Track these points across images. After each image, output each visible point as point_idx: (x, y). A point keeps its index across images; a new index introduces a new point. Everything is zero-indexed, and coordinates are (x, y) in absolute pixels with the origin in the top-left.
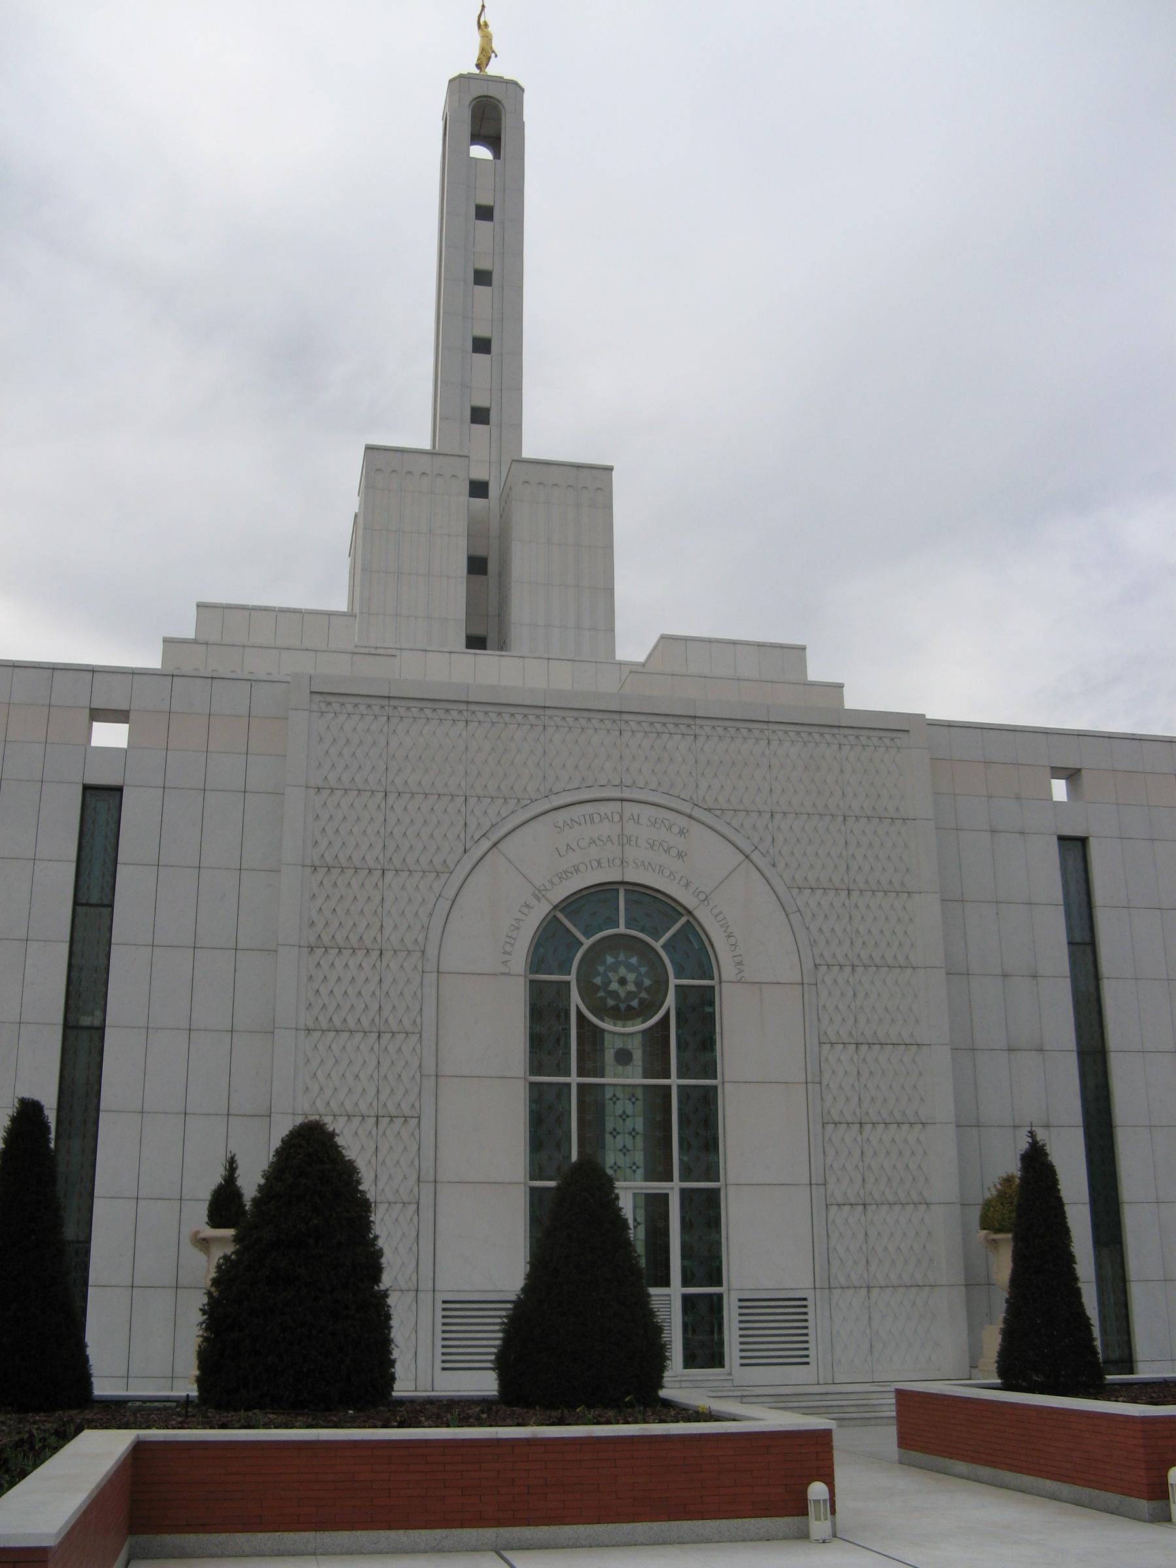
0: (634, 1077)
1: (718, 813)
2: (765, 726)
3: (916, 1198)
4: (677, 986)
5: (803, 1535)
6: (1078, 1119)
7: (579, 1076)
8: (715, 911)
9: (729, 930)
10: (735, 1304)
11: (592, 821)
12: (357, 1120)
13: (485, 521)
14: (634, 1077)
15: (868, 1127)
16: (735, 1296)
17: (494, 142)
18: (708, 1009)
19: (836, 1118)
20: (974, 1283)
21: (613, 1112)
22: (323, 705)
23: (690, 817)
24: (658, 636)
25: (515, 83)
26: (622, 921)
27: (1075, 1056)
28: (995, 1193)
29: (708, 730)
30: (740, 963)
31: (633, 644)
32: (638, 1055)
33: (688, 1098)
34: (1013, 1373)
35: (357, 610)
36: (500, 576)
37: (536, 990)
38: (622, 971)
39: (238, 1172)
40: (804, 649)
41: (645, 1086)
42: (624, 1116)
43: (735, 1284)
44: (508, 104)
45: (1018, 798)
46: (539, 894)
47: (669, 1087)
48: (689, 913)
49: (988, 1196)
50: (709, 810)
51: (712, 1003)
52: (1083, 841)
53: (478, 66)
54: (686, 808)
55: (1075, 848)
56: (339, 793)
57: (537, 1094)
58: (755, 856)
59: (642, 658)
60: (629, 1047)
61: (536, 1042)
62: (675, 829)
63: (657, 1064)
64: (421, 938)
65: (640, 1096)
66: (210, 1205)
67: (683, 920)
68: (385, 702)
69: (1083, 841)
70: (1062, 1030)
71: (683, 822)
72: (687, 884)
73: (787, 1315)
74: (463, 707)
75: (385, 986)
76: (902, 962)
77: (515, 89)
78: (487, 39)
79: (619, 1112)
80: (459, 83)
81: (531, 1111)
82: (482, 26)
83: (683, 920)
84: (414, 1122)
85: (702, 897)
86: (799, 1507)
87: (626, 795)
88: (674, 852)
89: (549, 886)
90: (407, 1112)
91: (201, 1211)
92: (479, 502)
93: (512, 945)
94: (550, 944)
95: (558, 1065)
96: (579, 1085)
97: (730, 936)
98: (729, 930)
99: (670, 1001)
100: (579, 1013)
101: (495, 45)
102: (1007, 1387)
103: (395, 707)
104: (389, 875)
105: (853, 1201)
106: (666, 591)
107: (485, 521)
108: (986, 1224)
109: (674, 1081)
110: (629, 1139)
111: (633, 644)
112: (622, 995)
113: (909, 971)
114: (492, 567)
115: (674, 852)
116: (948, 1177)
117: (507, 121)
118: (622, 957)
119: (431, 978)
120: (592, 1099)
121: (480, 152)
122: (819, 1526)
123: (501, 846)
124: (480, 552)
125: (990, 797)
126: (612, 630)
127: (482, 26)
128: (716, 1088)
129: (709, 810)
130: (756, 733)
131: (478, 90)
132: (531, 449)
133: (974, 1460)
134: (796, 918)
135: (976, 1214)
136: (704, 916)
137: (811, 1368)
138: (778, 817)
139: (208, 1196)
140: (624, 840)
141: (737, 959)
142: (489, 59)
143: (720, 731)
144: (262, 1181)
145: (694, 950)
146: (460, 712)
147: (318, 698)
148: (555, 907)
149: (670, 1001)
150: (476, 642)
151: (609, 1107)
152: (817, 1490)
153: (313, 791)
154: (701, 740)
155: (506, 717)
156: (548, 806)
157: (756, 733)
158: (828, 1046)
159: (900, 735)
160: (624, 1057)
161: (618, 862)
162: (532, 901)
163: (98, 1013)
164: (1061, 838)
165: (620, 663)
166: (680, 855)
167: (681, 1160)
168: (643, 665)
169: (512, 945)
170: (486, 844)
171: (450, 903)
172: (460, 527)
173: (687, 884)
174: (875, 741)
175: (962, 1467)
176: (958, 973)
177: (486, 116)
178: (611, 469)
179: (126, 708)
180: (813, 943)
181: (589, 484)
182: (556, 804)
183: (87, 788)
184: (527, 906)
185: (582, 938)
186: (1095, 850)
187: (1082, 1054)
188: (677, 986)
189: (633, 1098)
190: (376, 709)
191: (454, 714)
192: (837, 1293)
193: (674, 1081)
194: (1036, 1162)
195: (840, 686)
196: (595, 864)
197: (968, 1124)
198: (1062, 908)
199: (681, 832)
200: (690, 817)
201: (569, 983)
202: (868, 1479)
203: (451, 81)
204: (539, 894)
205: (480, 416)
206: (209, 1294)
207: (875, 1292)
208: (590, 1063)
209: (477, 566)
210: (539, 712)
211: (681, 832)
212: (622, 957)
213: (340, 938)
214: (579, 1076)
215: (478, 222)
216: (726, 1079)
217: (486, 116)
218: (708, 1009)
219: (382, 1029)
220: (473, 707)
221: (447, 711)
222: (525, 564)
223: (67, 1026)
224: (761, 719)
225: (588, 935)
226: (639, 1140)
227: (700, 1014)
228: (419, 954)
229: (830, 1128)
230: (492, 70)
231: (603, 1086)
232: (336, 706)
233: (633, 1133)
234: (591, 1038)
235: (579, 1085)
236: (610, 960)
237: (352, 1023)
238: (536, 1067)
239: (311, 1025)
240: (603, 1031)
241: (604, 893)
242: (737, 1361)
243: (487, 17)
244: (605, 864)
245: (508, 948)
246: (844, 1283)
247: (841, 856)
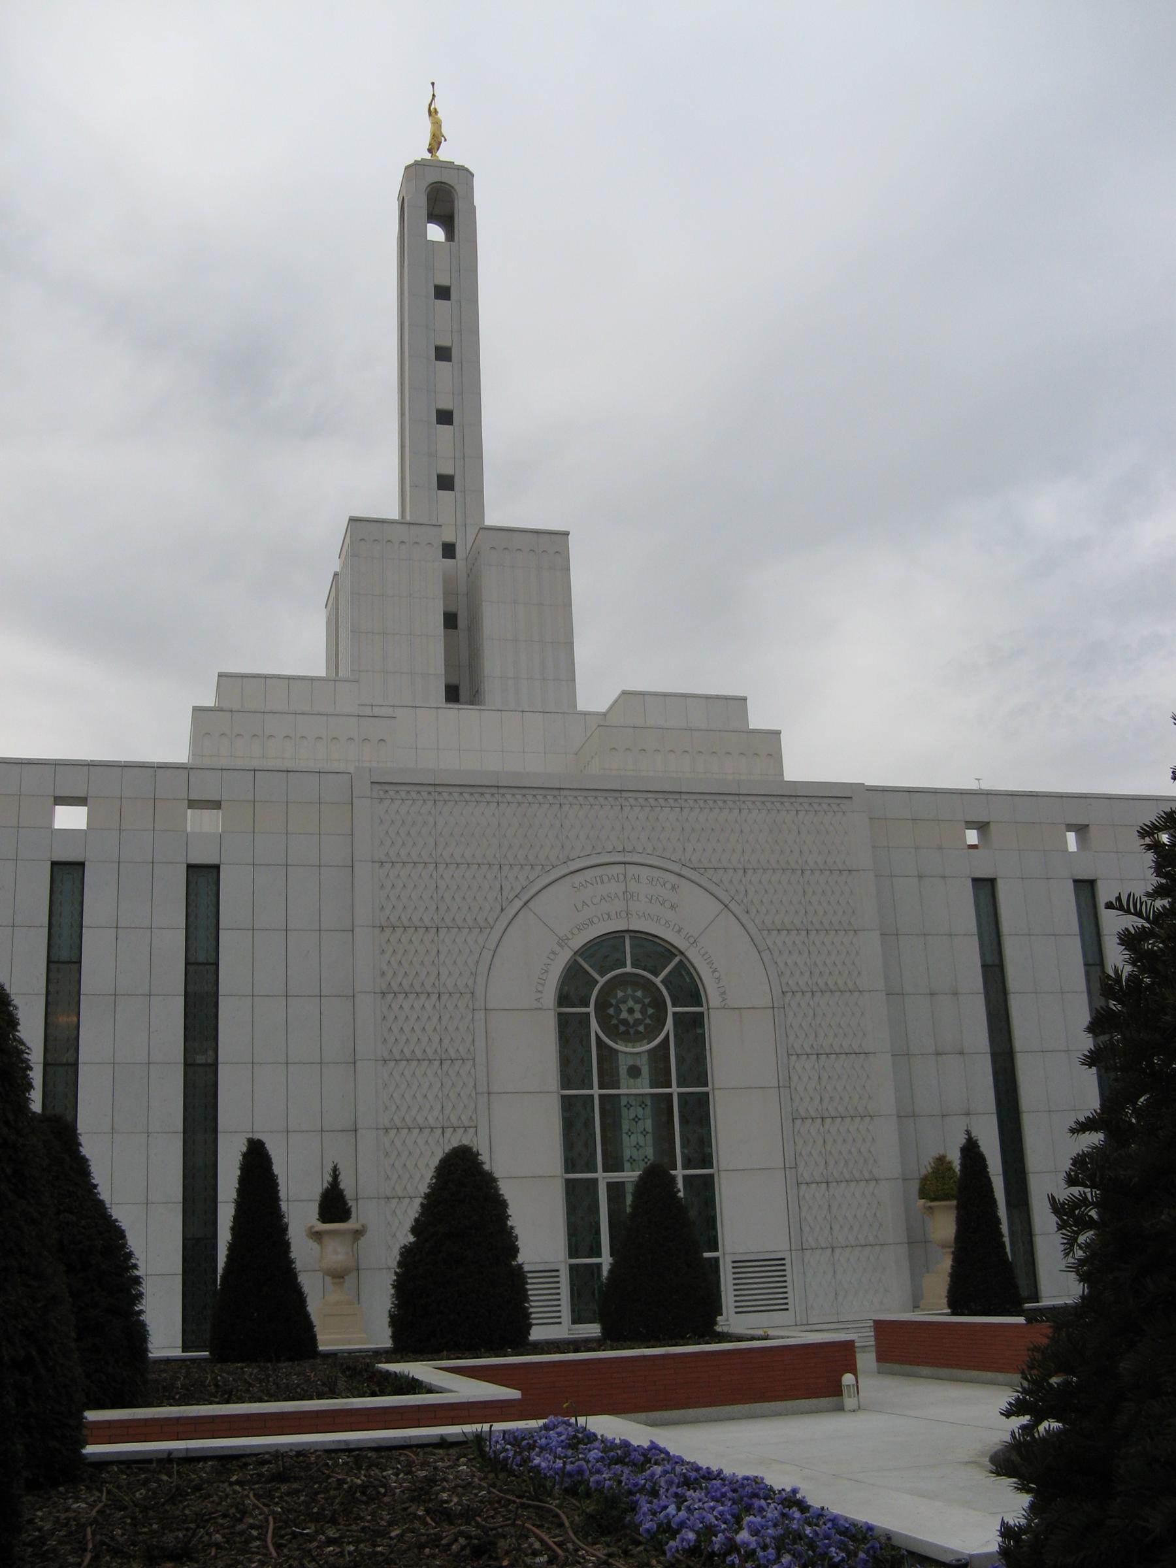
0: (643, 1088)
1: (702, 871)
2: (737, 798)
3: (867, 1176)
4: (675, 1014)
5: (840, 1409)
6: (992, 1106)
7: (600, 1088)
8: (702, 952)
9: (714, 966)
10: (729, 1265)
11: (602, 882)
12: (427, 1131)
13: (455, 588)
14: (643, 1088)
15: (828, 1121)
16: (729, 1259)
17: (447, 220)
18: (699, 1031)
19: (803, 1114)
20: (916, 1242)
21: (627, 1115)
22: (381, 793)
23: (679, 875)
24: (618, 692)
25: (467, 170)
26: (629, 962)
27: (989, 1056)
28: (930, 1170)
29: (691, 803)
30: (724, 993)
31: (595, 693)
32: (645, 1070)
33: (686, 1102)
34: (957, 1303)
35: (345, 672)
36: (469, 629)
37: (563, 1022)
38: (631, 1003)
39: (340, 1178)
40: (744, 699)
41: (652, 1095)
42: (636, 1119)
43: (728, 1249)
44: (460, 190)
45: (940, 848)
46: (562, 942)
47: (671, 1095)
48: (682, 953)
49: (923, 1172)
50: (694, 869)
51: (702, 1025)
52: (992, 882)
53: (430, 151)
54: (676, 868)
55: (985, 887)
56: (398, 866)
57: (568, 1104)
58: (732, 906)
59: (603, 708)
60: (638, 1064)
61: (565, 1062)
62: (668, 886)
63: (661, 1077)
64: (470, 982)
65: (649, 1102)
66: (321, 1206)
67: (677, 960)
68: (431, 789)
69: (992, 882)
70: (978, 1037)
71: (673, 879)
72: (679, 931)
73: (769, 1272)
74: (494, 790)
75: (444, 1023)
76: (851, 987)
77: (466, 174)
78: (437, 124)
79: (632, 1116)
80: (414, 170)
81: (564, 1118)
82: (432, 113)
83: (677, 960)
84: (472, 1131)
85: (692, 940)
86: (836, 1390)
87: (627, 859)
88: (668, 905)
89: (570, 936)
90: (467, 1124)
91: (314, 1209)
92: (449, 562)
93: (543, 985)
94: (573, 986)
95: (583, 1081)
96: (601, 1096)
97: (715, 971)
98: (714, 966)
99: (669, 1024)
100: (597, 1037)
101: (444, 131)
102: (954, 1314)
103: (440, 793)
104: (443, 932)
105: (818, 1179)
106: (619, 648)
107: (455, 588)
108: (923, 1194)
109: (675, 1090)
110: (641, 1138)
111: (595, 693)
112: (631, 1022)
113: (856, 994)
114: (462, 622)
115: (668, 905)
116: (887, 1161)
117: (460, 206)
118: (629, 991)
119: (480, 1015)
120: (611, 1106)
121: (435, 233)
122: (849, 1402)
123: (531, 904)
124: (452, 609)
125: (917, 848)
126: (573, 680)
127: (432, 113)
128: (707, 1094)
129: (694, 869)
130: (730, 804)
131: (433, 177)
132: (493, 518)
133: (933, 1364)
134: (766, 955)
135: (915, 1186)
136: (693, 955)
137: (790, 1313)
138: (750, 872)
139: (318, 1197)
140: (628, 896)
141: (722, 990)
142: (440, 143)
143: (701, 803)
144: (428, 1191)
145: (688, 989)
146: (493, 795)
147: (378, 787)
148: (575, 953)
149: (669, 1024)
150: (453, 694)
151: (624, 1111)
152: (848, 1379)
153: (377, 865)
154: (686, 811)
155: (530, 798)
156: (567, 871)
157: (730, 804)
158: (794, 1058)
159: (845, 801)
160: (634, 1072)
161: (624, 915)
162: (557, 949)
163: (210, 1053)
164: (1075, 881)
165: (585, 714)
166: (672, 907)
167: (682, 1153)
168: (605, 715)
169: (543, 985)
170: (518, 904)
171: (491, 953)
172: (436, 589)
173: (679, 931)
174: (825, 806)
175: (927, 1370)
176: (894, 994)
177: (439, 198)
178: (567, 534)
179: (217, 798)
180: (780, 975)
181: (548, 549)
182: (572, 868)
183: (190, 867)
184: (553, 952)
185: (597, 976)
186: (1001, 886)
187: (995, 1055)
188: (675, 1014)
189: (643, 1105)
190: (424, 794)
191: (488, 797)
192: (808, 1252)
193: (675, 1090)
194: (971, 1150)
195: (778, 733)
196: (606, 917)
197: (906, 1115)
198: (976, 938)
199: (673, 888)
200: (679, 875)
201: (588, 1014)
202: (869, 1381)
203: (407, 168)
204: (562, 942)
205: (446, 483)
206: (396, 1273)
207: (838, 1251)
208: (609, 1078)
209: (450, 621)
210: (556, 793)
211: (673, 888)
212: (629, 991)
213: (406, 984)
214: (600, 1088)
215: (438, 301)
216: (716, 1086)
217: (439, 198)
218: (699, 1031)
219: (444, 1057)
220: (502, 791)
221: (482, 794)
222: (496, 622)
223: (185, 1064)
224: (709, 771)
225: (602, 975)
226: (649, 1138)
227: (693, 1029)
228: (469, 995)
229: (798, 1122)
230: (443, 154)
231: (619, 1095)
232: (392, 793)
233: (644, 1133)
234: (607, 1056)
235: (601, 1096)
236: (620, 994)
237: (408, 1054)
238: (566, 1082)
239: (386, 1056)
240: (617, 1051)
241: (613, 940)
242: (732, 1310)
243: (437, 104)
244: (613, 915)
245: (540, 988)
246: (813, 1245)
247: (800, 903)
